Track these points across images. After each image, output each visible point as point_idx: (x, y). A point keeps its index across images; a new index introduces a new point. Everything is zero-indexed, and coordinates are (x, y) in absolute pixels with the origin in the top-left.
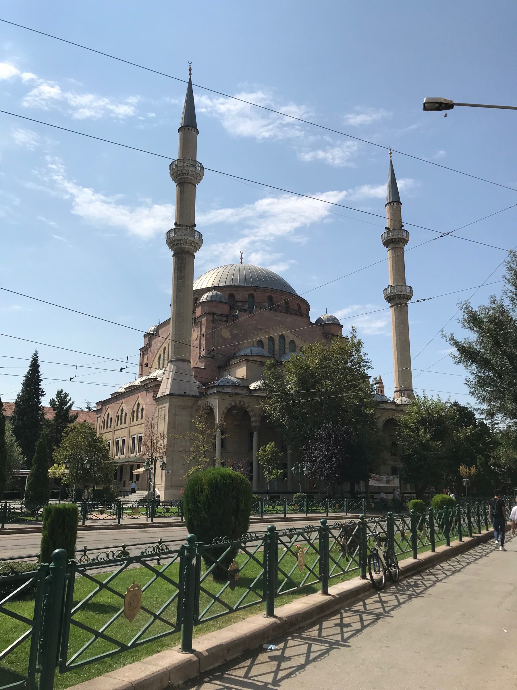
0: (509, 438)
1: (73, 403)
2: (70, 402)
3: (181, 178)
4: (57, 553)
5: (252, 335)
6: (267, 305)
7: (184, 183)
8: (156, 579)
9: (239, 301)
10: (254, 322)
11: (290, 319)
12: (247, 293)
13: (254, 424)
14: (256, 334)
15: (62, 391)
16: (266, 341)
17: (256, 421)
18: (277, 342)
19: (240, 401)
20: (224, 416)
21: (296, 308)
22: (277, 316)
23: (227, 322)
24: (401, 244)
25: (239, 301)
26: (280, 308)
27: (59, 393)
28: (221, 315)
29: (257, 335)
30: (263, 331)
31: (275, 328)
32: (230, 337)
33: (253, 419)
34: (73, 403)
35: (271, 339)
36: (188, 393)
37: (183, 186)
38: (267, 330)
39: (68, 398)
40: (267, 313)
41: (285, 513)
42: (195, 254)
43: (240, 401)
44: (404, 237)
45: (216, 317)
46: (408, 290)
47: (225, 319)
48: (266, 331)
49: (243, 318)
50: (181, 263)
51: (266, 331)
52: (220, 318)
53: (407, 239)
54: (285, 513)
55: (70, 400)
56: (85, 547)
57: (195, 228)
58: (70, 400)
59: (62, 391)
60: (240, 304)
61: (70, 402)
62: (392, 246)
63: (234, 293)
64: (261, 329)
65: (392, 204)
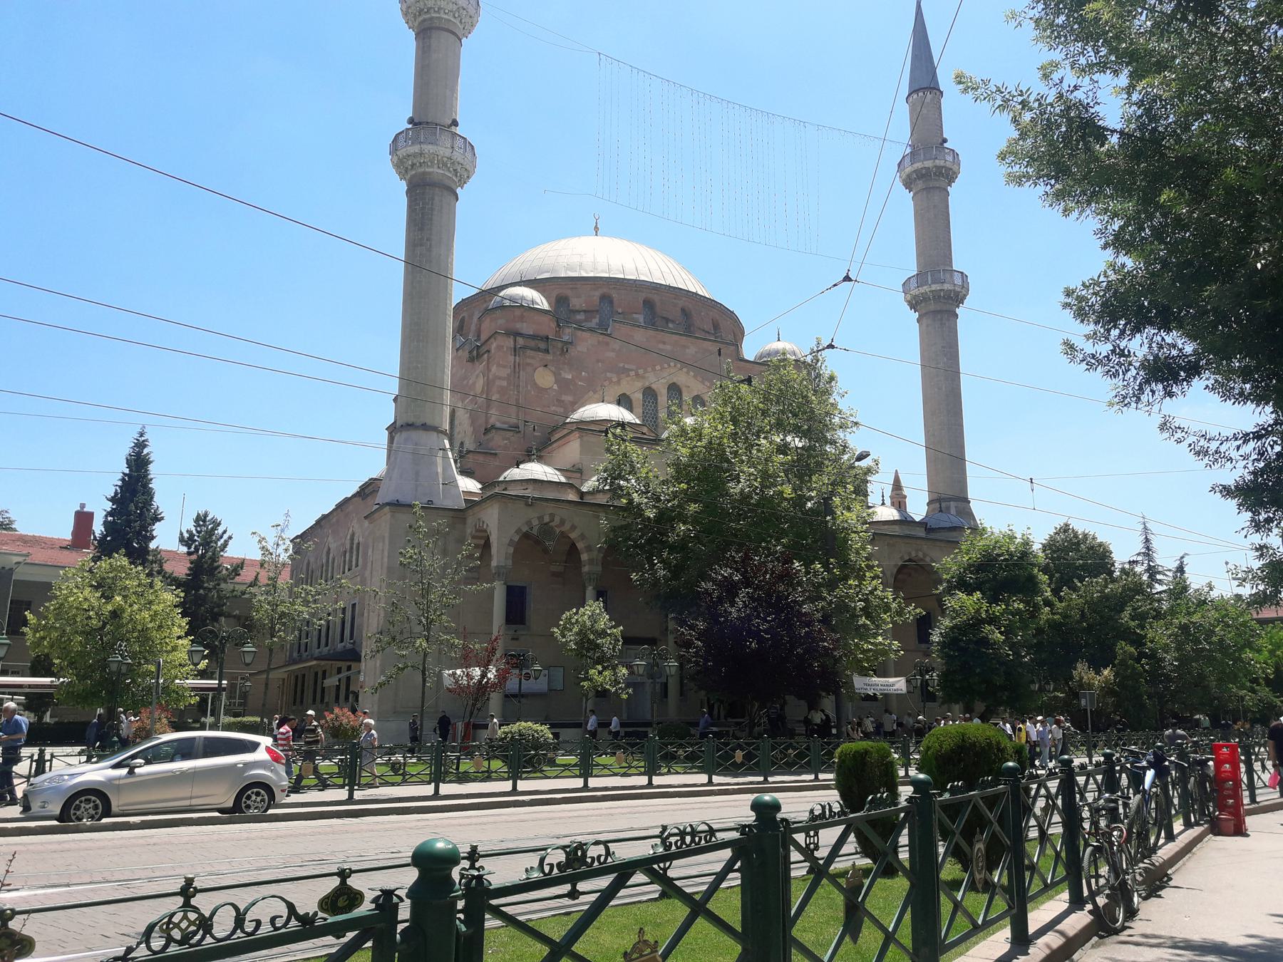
0: (1163, 155)
1: (230, 538)
2: (225, 537)
3: (424, 20)
4: (936, 847)
5: (606, 383)
6: (641, 318)
7: (430, 29)
8: (655, 900)
9: (579, 312)
10: (612, 355)
11: (692, 349)
12: (597, 294)
13: (586, 569)
14: (615, 379)
15: (206, 515)
16: (637, 397)
17: (591, 561)
18: (663, 399)
19: (552, 516)
20: (511, 550)
21: (708, 326)
22: (664, 343)
23: (547, 351)
24: (942, 182)
25: (579, 312)
26: (671, 325)
27: (201, 519)
28: (534, 337)
29: (619, 382)
30: (632, 373)
31: (658, 367)
32: (555, 387)
33: (584, 557)
34: (230, 538)
35: (650, 393)
36: (438, 503)
37: (430, 38)
38: (641, 372)
39: (220, 530)
40: (640, 336)
41: (586, 773)
42: (459, 190)
43: (552, 516)
44: (948, 164)
45: (521, 341)
46: (958, 281)
47: (542, 345)
48: (637, 375)
49: (586, 343)
50: (423, 208)
51: (637, 375)
52: (532, 343)
53: (955, 168)
54: (586, 773)
55: (225, 532)
56: (474, 849)
57: (458, 130)
58: (225, 532)
59: (206, 515)
60: (581, 317)
61: (225, 537)
62: (920, 184)
63: (569, 293)
64: (626, 371)
65: (921, 94)
